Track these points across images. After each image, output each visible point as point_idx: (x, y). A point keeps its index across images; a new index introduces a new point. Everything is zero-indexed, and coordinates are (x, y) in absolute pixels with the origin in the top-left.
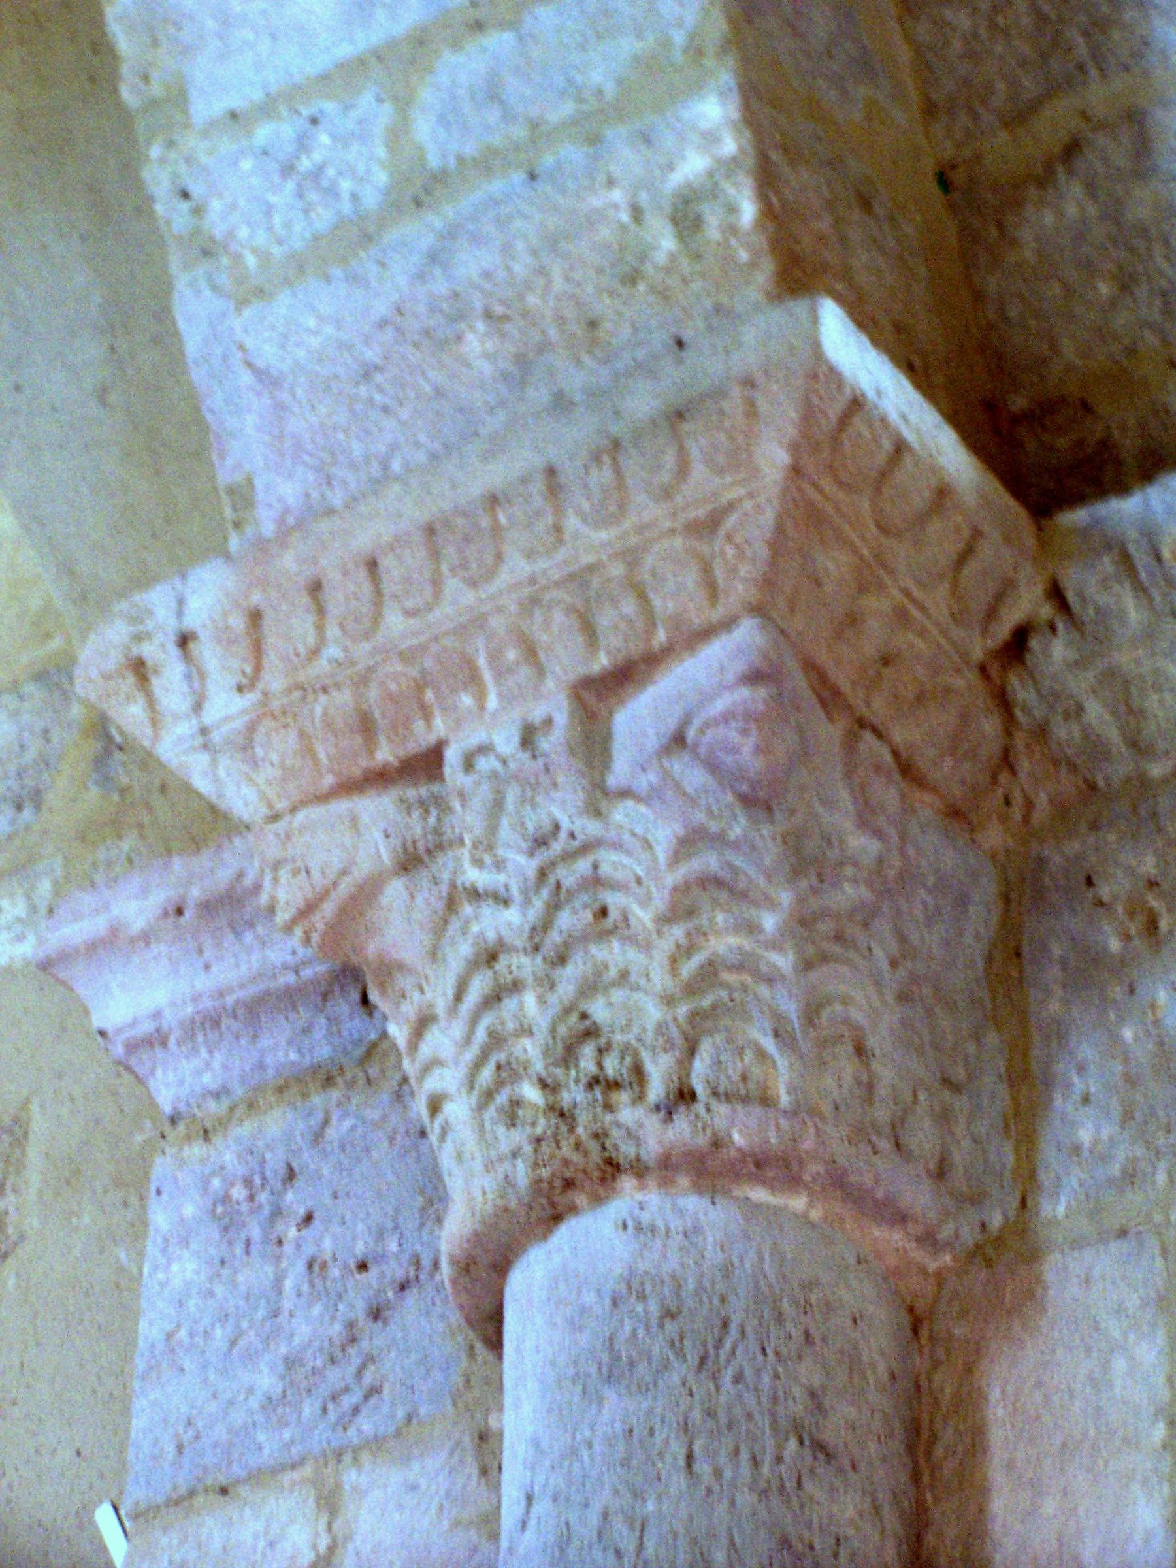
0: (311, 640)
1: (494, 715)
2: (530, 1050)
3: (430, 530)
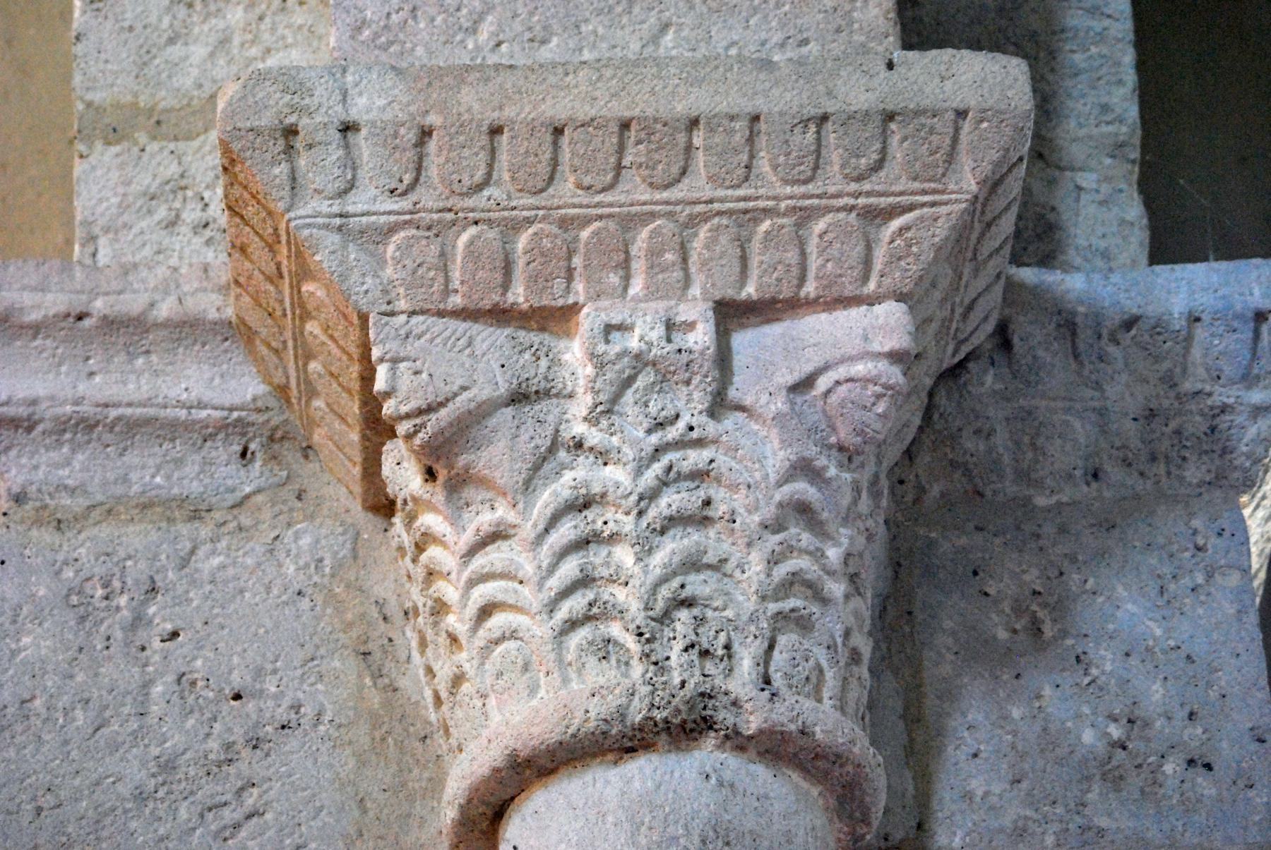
0: (479, 175)
1: (637, 300)
2: (627, 598)
3: (625, 125)
